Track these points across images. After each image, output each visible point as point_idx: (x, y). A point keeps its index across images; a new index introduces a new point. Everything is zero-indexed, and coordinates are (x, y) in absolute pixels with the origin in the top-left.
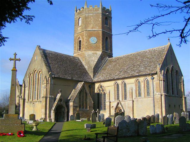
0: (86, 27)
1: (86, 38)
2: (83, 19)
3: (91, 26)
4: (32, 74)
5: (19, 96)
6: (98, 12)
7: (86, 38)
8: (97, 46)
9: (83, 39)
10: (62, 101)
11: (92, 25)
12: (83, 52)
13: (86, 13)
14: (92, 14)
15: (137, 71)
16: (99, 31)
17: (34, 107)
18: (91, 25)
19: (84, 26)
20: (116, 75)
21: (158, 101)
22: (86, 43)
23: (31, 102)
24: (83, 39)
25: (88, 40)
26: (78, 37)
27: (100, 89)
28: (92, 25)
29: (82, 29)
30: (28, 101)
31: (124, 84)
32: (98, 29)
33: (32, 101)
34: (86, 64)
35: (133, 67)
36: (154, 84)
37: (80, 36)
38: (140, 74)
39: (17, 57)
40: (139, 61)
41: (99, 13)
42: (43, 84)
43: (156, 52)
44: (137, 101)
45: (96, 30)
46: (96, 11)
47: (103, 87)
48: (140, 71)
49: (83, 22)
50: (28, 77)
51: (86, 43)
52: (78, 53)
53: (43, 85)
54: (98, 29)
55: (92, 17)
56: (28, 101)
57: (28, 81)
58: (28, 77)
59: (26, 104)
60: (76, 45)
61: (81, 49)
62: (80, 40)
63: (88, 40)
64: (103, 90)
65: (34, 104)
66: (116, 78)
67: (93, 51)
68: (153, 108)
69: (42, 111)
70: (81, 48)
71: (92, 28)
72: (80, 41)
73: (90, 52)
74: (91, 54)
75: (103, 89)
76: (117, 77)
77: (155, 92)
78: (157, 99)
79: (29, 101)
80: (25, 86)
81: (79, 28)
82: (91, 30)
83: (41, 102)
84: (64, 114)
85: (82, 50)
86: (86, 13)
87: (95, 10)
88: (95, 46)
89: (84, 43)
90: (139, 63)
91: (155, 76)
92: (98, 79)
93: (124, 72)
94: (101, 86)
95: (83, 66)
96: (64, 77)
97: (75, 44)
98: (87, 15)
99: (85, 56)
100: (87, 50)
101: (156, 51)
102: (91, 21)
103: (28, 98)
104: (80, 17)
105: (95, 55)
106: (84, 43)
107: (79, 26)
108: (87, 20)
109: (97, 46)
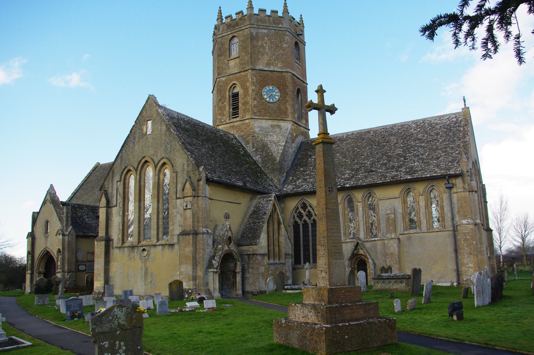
0: (253, 60)
1: (254, 88)
2: (244, 41)
3: (266, 59)
4: (136, 170)
5: (62, 231)
6: (280, 26)
7: (254, 88)
8: (279, 108)
9: (246, 89)
10: (231, 242)
11: (266, 58)
12: (247, 121)
13: (252, 26)
14: (266, 31)
15: (403, 169)
16: (284, 74)
17: (145, 260)
18: (265, 56)
19: (247, 58)
20: (345, 179)
21: (468, 237)
22: (255, 99)
23: (133, 247)
24: (246, 89)
25: (259, 95)
26: (231, 84)
27: (300, 213)
28: (266, 58)
29: (241, 64)
30: (120, 245)
31: (348, 199)
32: (280, 68)
33: (135, 244)
34: (256, 151)
35: (389, 161)
36: (455, 200)
37: (235, 82)
38: (416, 176)
39: (328, 102)
40: (399, 148)
41: (283, 29)
42: (177, 198)
43: (438, 127)
44: (409, 238)
45: (276, 69)
46: (274, 23)
47: (309, 208)
48: (412, 171)
49: (243, 48)
50: (117, 178)
51: (255, 99)
52: (232, 124)
53: (178, 201)
54: (280, 68)
55: (267, 36)
56: (120, 245)
57: (121, 190)
58: (117, 178)
59: (115, 253)
60: (223, 103)
61: (240, 115)
62: (235, 91)
63: (259, 95)
64: (309, 215)
65: (145, 253)
66: (348, 185)
67: (270, 121)
68: (453, 255)
69: (183, 270)
70: (240, 111)
71: (268, 64)
72: (235, 96)
73: (266, 124)
74: (268, 128)
75: (309, 212)
76: (352, 183)
77: (457, 219)
78: (465, 234)
79: (126, 244)
80: (108, 202)
81: (232, 63)
82: (266, 69)
83: (172, 245)
84: (235, 277)
85: (243, 117)
86: (252, 26)
87: (274, 20)
88: (275, 109)
89: (249, 99)
90: (399, 151)
91: (458, 182)
92: (293, 188)
93: (365, 172)
94: (304, 204)
95: (249, 156)
96: (230, 180)
97: (220, 100)
98: (254, 31)
99: (254, 132)
100: (256, 117)
101: (437, 124)
102: (264, 48)
103: (120, 237)
104: (235, 34)
105: (278, 130)
106: (247, 100)
107: (232, 58)
108: (255, 43)
109: (279, 108)
